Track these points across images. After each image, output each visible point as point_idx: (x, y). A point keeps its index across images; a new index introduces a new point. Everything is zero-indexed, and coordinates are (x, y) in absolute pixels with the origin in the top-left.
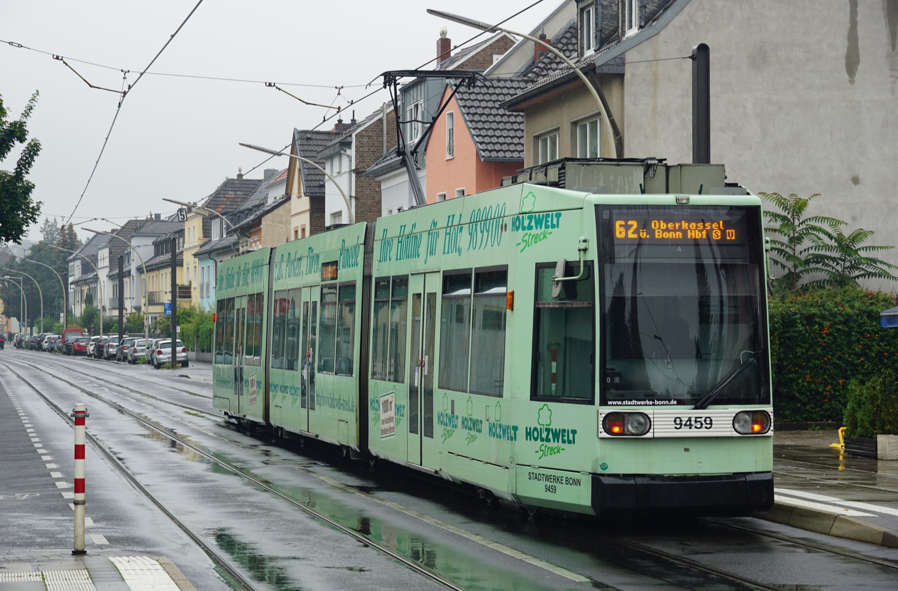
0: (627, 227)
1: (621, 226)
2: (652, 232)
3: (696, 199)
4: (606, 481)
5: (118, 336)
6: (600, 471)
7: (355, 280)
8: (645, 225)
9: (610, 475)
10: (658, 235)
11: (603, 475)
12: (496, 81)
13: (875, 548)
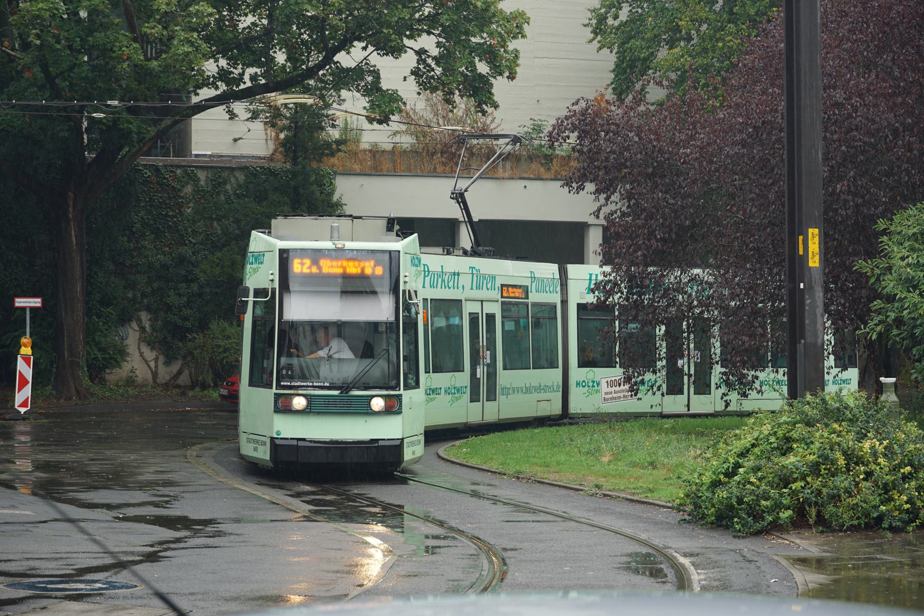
0: (302, 264)
1: (298, 263)
2: (320, 268)
3: (349, 245)
4: (277, 442)
5: (395, 473)
6: (275, 436)
7: (588, 264)
8: (315, 262)
9: (281, 439)
10: (325, 270)
11: (277, 438)
12: (430, 59)
13: (508, 510)
